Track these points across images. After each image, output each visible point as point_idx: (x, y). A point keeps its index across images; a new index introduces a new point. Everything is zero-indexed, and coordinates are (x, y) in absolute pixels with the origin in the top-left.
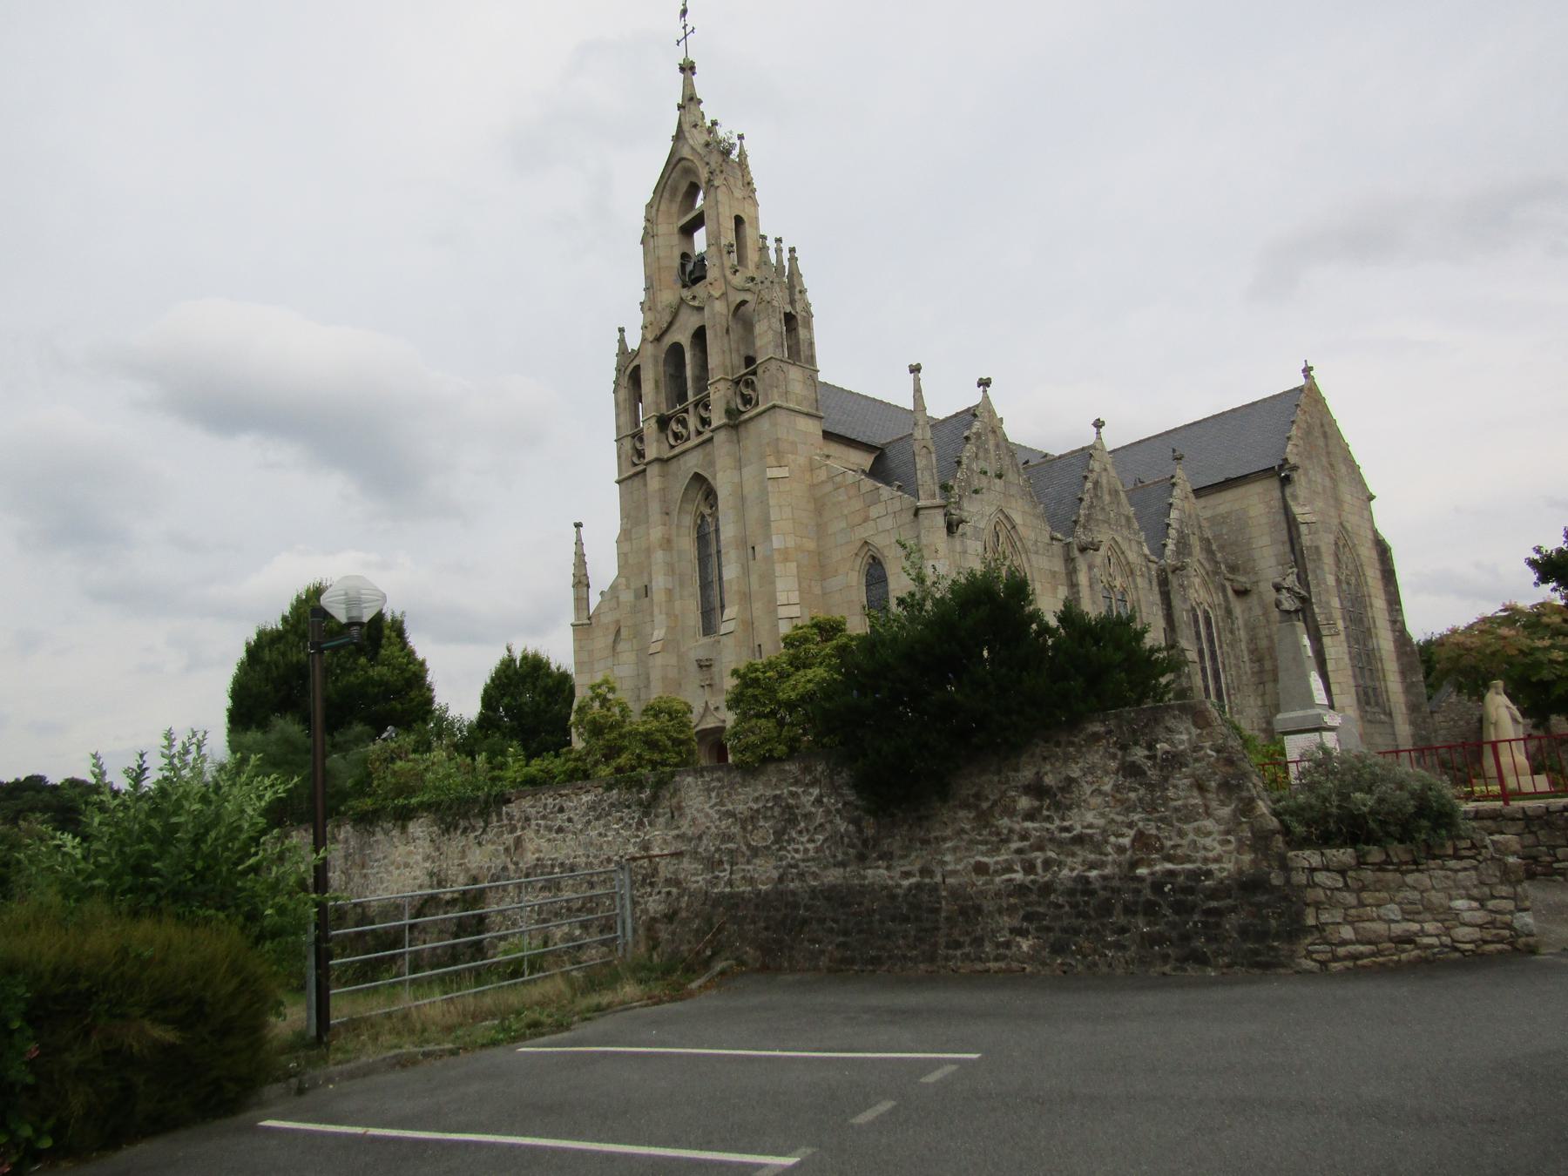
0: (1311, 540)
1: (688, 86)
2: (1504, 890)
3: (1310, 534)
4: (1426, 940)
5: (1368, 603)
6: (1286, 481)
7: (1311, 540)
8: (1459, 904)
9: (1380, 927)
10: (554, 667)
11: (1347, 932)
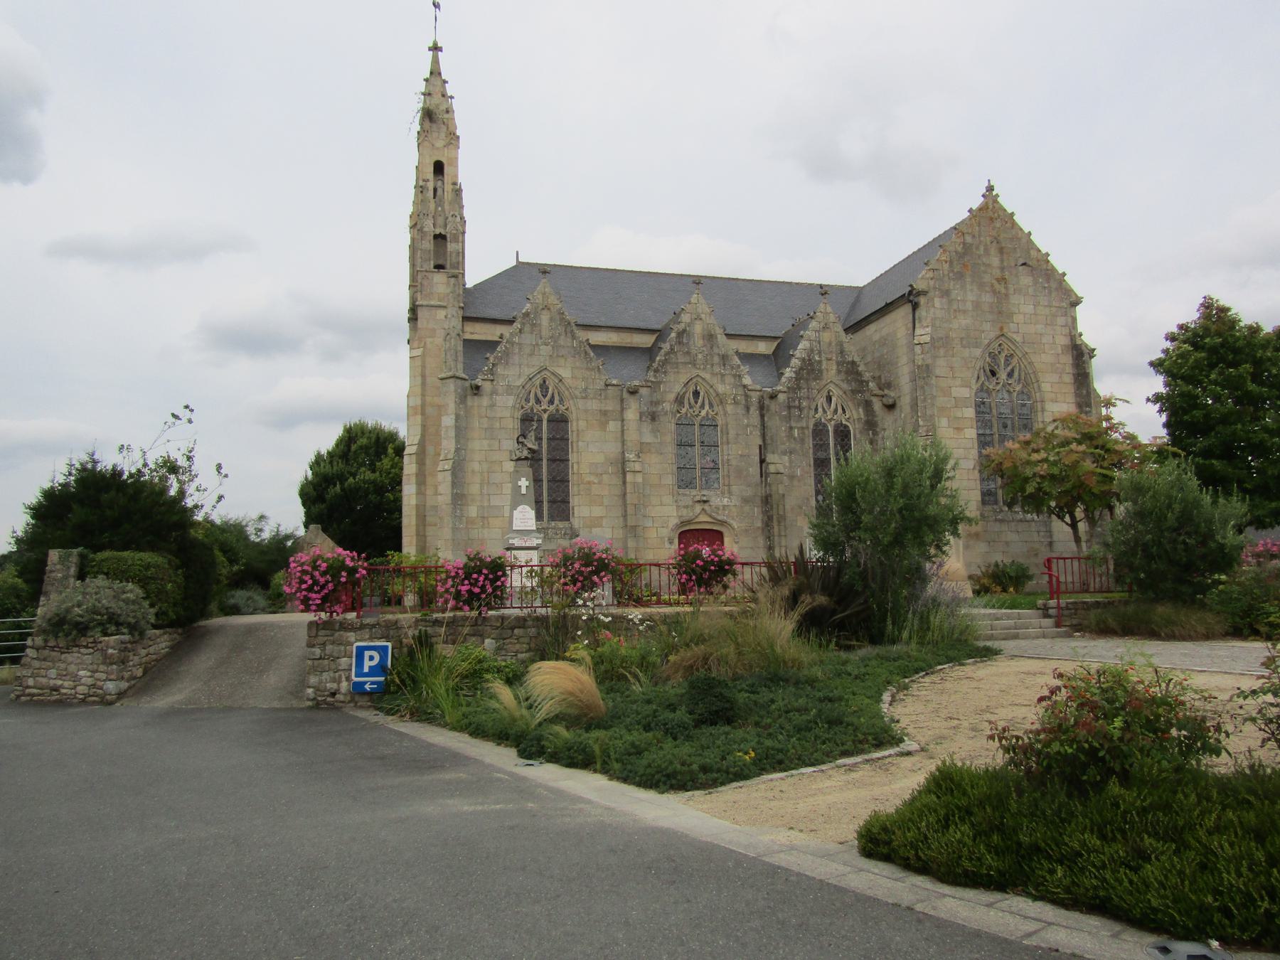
0: (923, 359)
1: (436, 61)
2: (102, 668)
3: (922, 353)
4: (64, 691)
5: (1039, 409)
6: (915, 307)
7: (923, 359)
8: (82, 673)
9: (44, 680)
10: (1164, 418)
11: (31, 682)
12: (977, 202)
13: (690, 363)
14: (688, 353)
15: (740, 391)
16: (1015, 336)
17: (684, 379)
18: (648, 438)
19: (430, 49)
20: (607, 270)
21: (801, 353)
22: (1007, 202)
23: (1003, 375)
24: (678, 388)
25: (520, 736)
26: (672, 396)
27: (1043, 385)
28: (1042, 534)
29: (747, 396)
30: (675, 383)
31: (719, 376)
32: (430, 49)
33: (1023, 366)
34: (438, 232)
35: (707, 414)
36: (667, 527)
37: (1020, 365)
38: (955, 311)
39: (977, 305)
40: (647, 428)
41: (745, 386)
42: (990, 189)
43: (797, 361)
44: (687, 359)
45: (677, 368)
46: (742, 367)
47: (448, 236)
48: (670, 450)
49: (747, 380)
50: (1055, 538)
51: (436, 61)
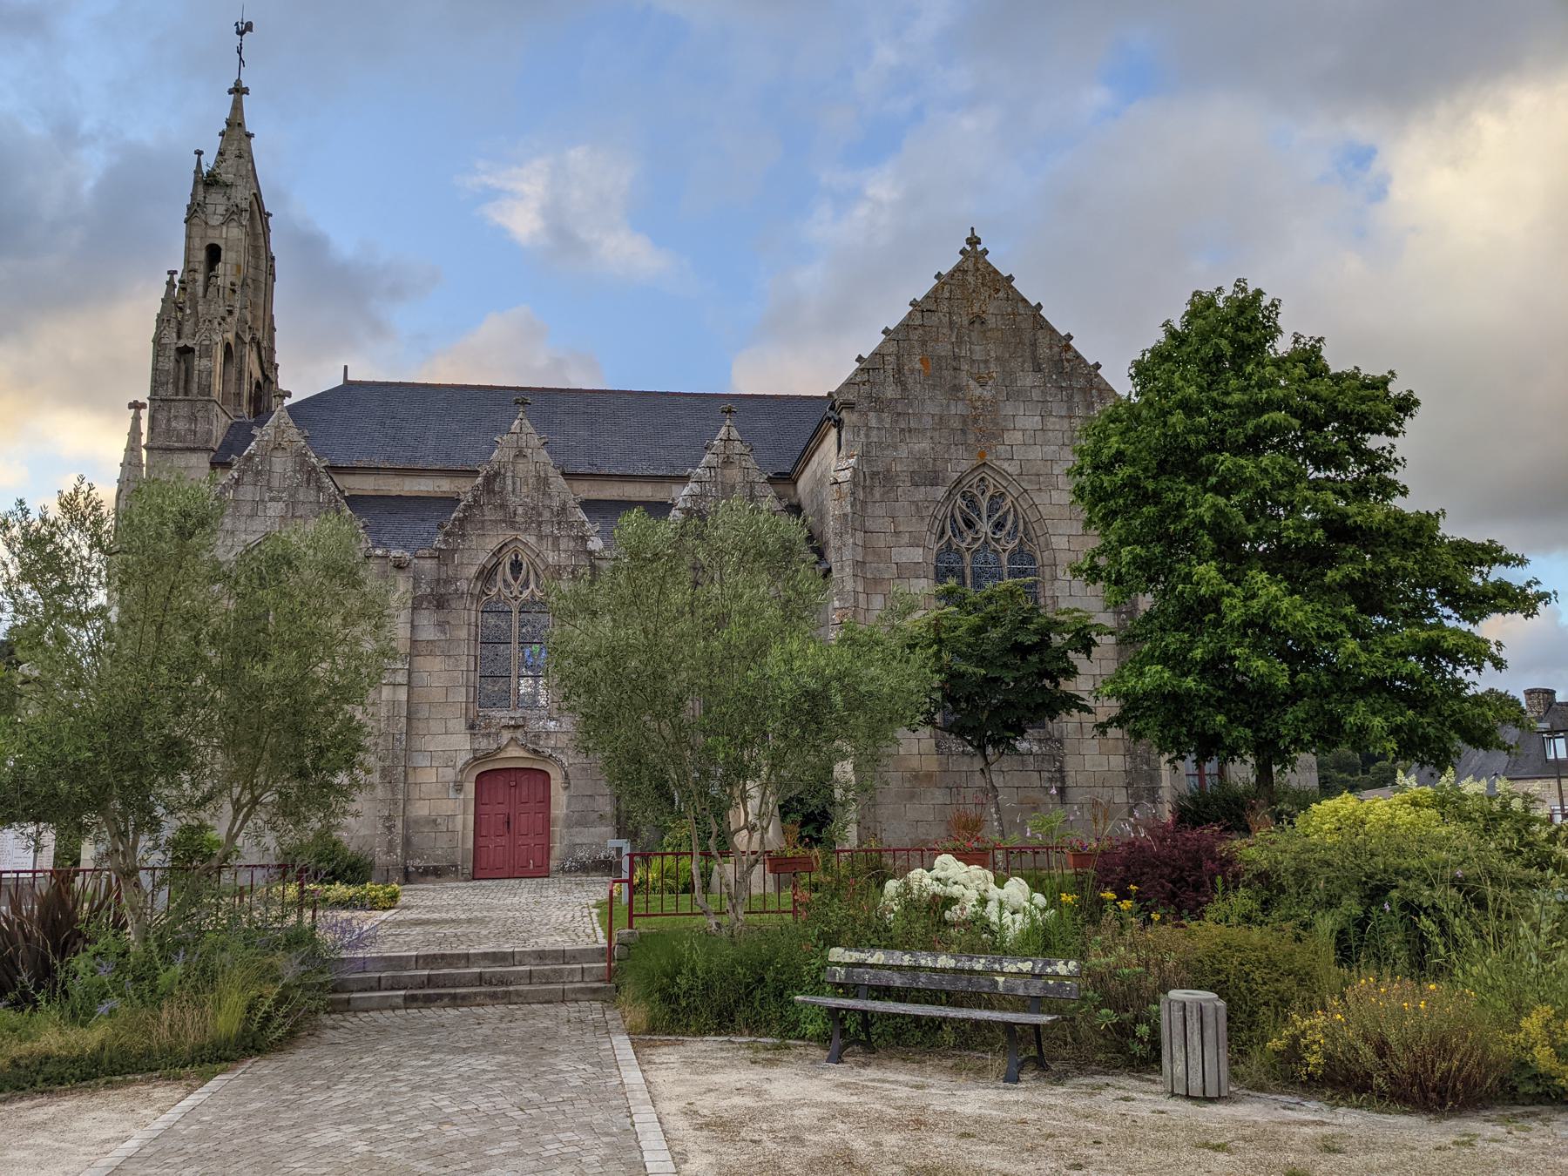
1: (237, 108)
5: (1048, 576)
12: (949, 261)
13: (504, 521)
14: (503, 506)
15: (584, 561)
16: (1005, 465)
17: (493, 543)
18: (428, 633)
19: (230, 92)
20: (479, 387)
21: (685, 501)
22: (1001, 259)
23: (985, 527)
24: (483, 558)
25: (668, 998)
26: (473, 571)
27: (1054, 539)
28: (1046, 775)
29: (593, 566)
30: (479, 550)
31: (550, 539)
32: (230, 92)
33: (1019, 509)
34: (181, 343)
35: (533, 595)
36: (454, 767)
37: (1015, 511)
38: (902, 430)
39: (941, 421)
40: (426, 619)
41: (591, 553)
42: (974, 241)
43: (677, 513)
44: (500, 515)
45: (483, 528)
46: (588, 525)
47: (197, 348)
48: (465, 653)
49: (596, 544)
50: (1069, 782)
51: (237, 108)
